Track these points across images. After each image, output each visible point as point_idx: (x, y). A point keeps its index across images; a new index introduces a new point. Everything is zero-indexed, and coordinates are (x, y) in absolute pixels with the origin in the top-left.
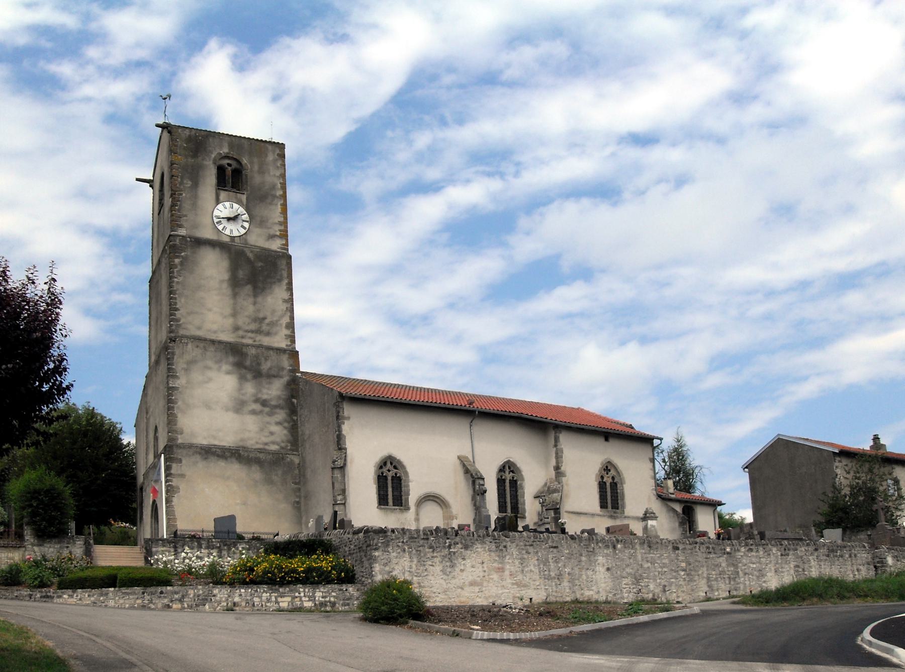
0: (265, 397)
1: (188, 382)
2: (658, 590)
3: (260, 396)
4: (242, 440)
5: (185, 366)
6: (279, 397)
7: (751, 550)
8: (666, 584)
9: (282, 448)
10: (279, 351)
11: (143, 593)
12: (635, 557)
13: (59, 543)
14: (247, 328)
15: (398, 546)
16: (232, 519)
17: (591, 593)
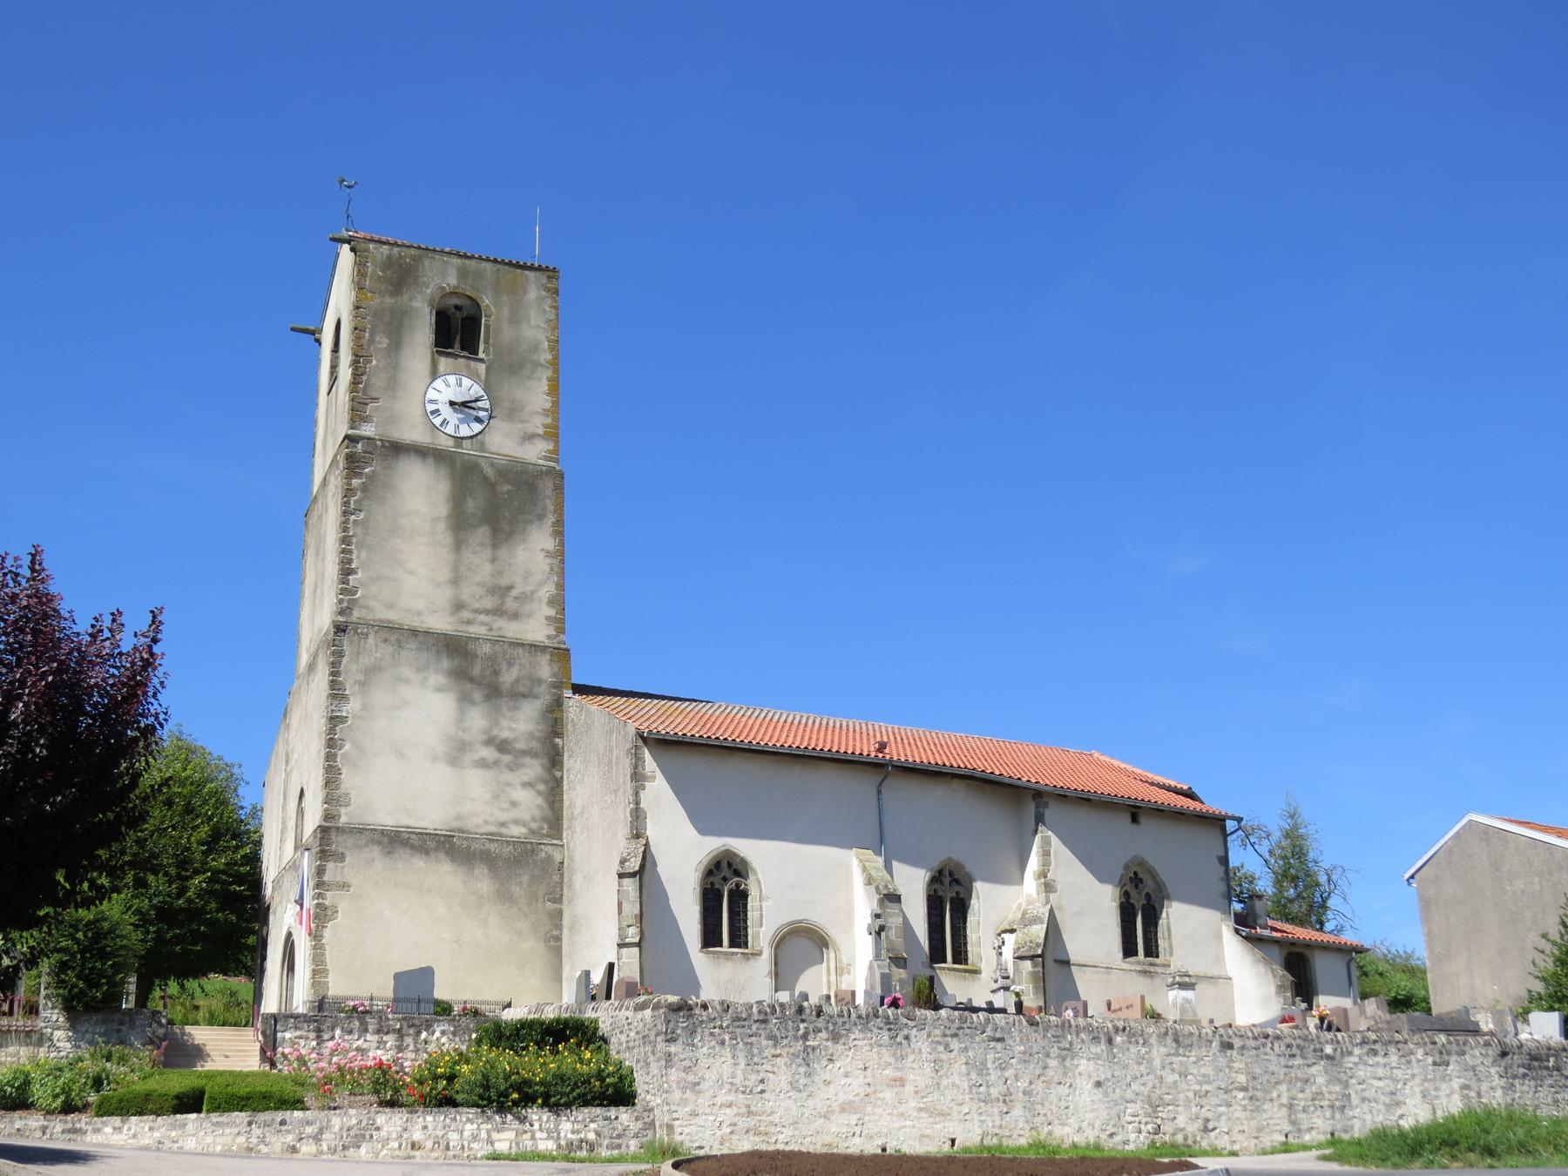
0: (505, 734)
1: (364, 707)
2: (1194, 1128)
3: (495, 732)
4: (458, 817)
5: (361, 677)
6: (531, 735)
7: (1375, 1053)
8: (1209, 1115)
9: (532, 832)
10: (535, 648)
11: (250, 1124)
12: (1150, 1061)
13: (104, 1022)
14: (477, 606)
15: (712, 1034)
16: (427, 973)
17: (1067, 1130)
